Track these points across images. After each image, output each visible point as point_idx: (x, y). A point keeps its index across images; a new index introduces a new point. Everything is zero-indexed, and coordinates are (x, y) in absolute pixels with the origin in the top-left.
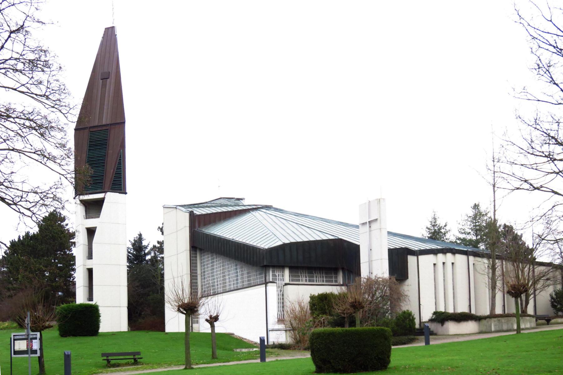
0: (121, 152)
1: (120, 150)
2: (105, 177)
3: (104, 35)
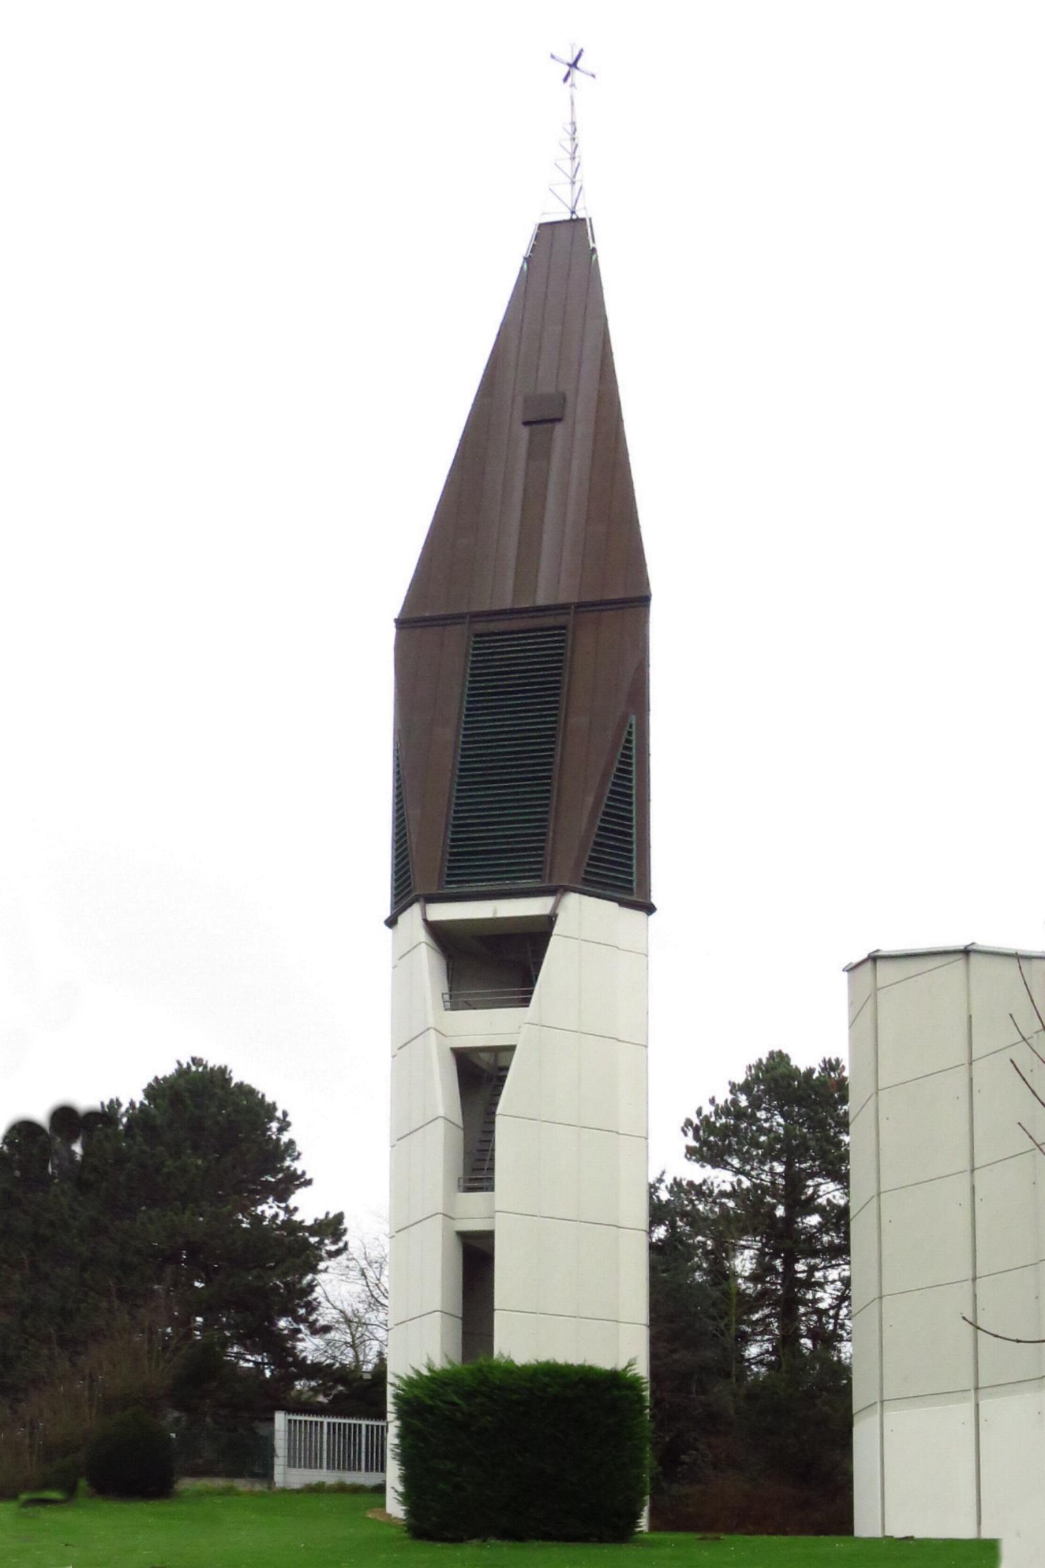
0: (631, 727)
1: (625, 717)
2: (563, 746)
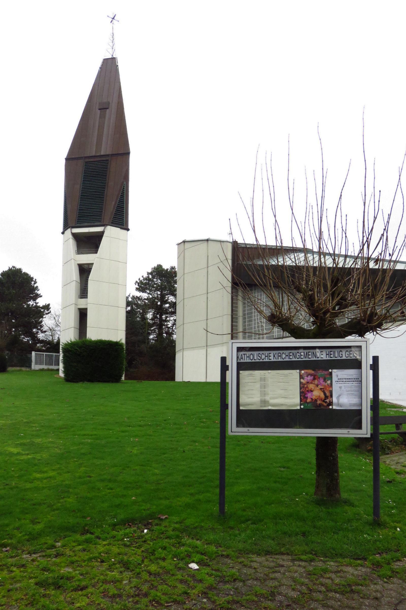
1: (123, 183)
3: (102, 65)
